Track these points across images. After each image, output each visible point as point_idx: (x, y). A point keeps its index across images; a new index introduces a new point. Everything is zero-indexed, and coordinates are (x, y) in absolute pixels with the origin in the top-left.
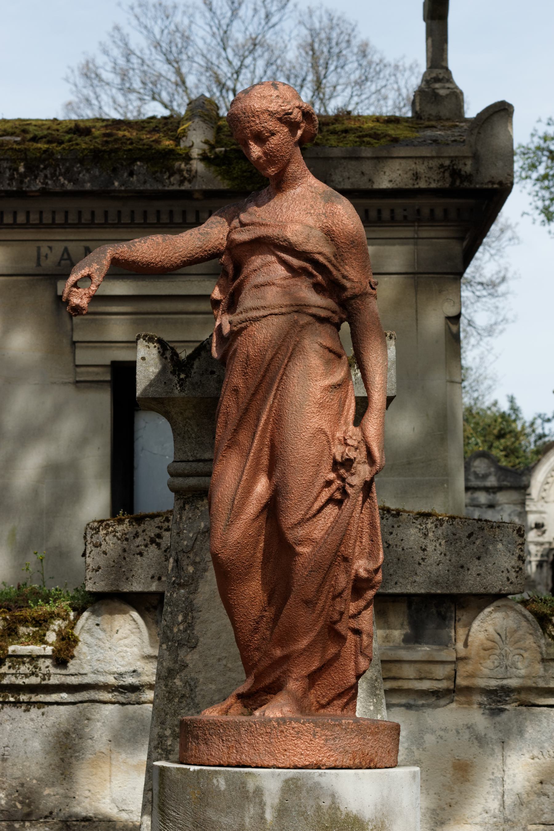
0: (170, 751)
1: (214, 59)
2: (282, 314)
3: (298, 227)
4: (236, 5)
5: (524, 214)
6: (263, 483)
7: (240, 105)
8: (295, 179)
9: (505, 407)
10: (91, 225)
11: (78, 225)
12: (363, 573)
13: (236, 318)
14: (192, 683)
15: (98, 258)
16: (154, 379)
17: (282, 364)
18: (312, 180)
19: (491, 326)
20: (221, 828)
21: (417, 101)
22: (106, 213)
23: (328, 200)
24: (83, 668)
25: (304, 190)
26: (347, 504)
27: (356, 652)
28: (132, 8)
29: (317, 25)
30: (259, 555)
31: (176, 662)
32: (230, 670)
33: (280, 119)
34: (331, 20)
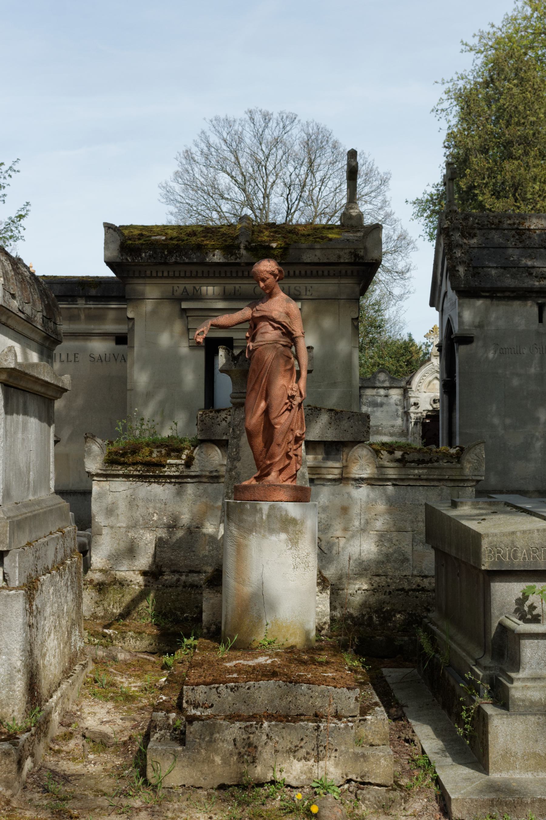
3: (277, 312)
5: (420, 236)
8: (276, 294)
9: (407, 338)
10: (196, 277)
11: (191, 277)
12: (298, 435)
13: (255, 344)
18: (282, 294)
19: (95, 586)
22: (203, 272)
23: (288, 301)
26: (293, 411)
28: (211, 121)
29: (311, 132)
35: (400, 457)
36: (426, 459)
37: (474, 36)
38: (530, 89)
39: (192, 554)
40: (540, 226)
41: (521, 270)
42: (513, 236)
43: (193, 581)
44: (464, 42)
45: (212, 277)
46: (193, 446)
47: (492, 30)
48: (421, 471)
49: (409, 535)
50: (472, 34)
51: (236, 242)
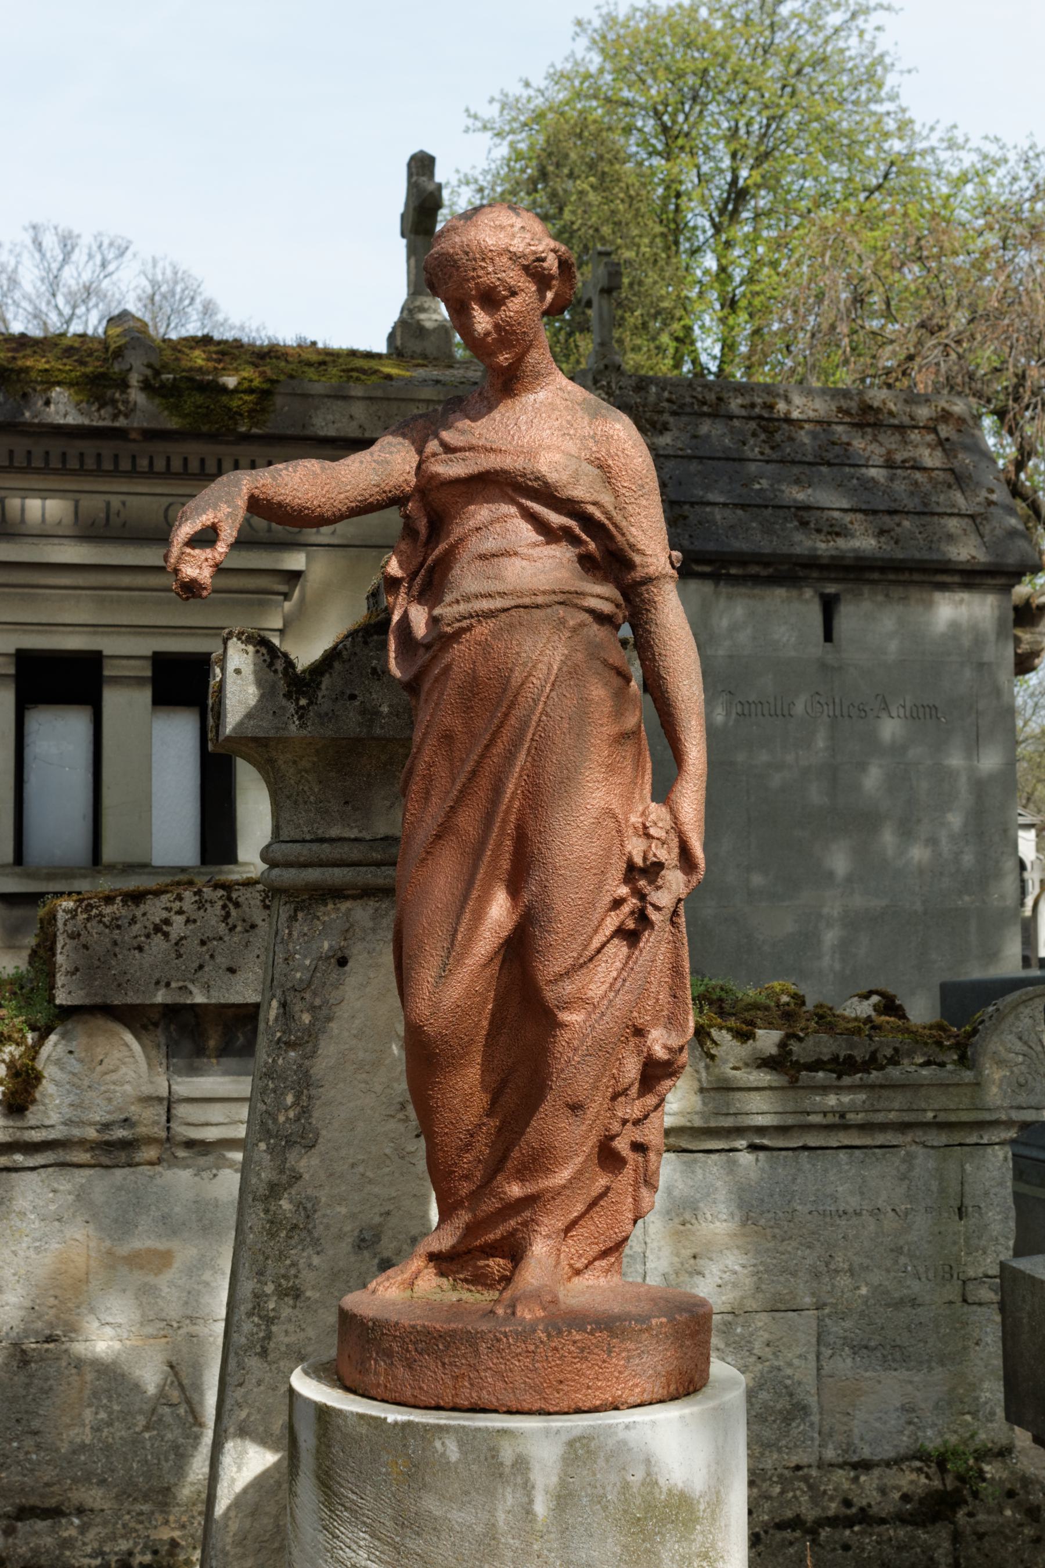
0: (274, 1318)
1: (44, 307)
3: (557, 457)
4: (69, 247)
6: (501, 901)
7: (457, 239)
8: (538, 376)
12: (660, 1053)
14: (309, 1206)
15: (228, 493)
16: (255, 706)
17: (540, 695)
20: (451, 1530)
21: (398, 333)
23: (595, 415)
24: (49, 1118)
25: (550, 395)
27: (636, 1181)
29: (160, 277)
30: (485, 1023)
31: (282, 1172)
32: (370, 1182)
33: (526, 268)
34: (176, 273)
35: (774, 1051)
36: (860, 1054)
37: (492, 100)
38: (622, 195)
39: (29, 1442)
40: (811, 414)
41: (781, 513)
42: (754, 435)
43: (36, 1552)
44: (472, 112)
45: (38, 471)
46: (33, 1028)
47: (526, 93)
48: (846, 1099)
49: (806, 1323)
50: (488, 98)
51: (116, 368)
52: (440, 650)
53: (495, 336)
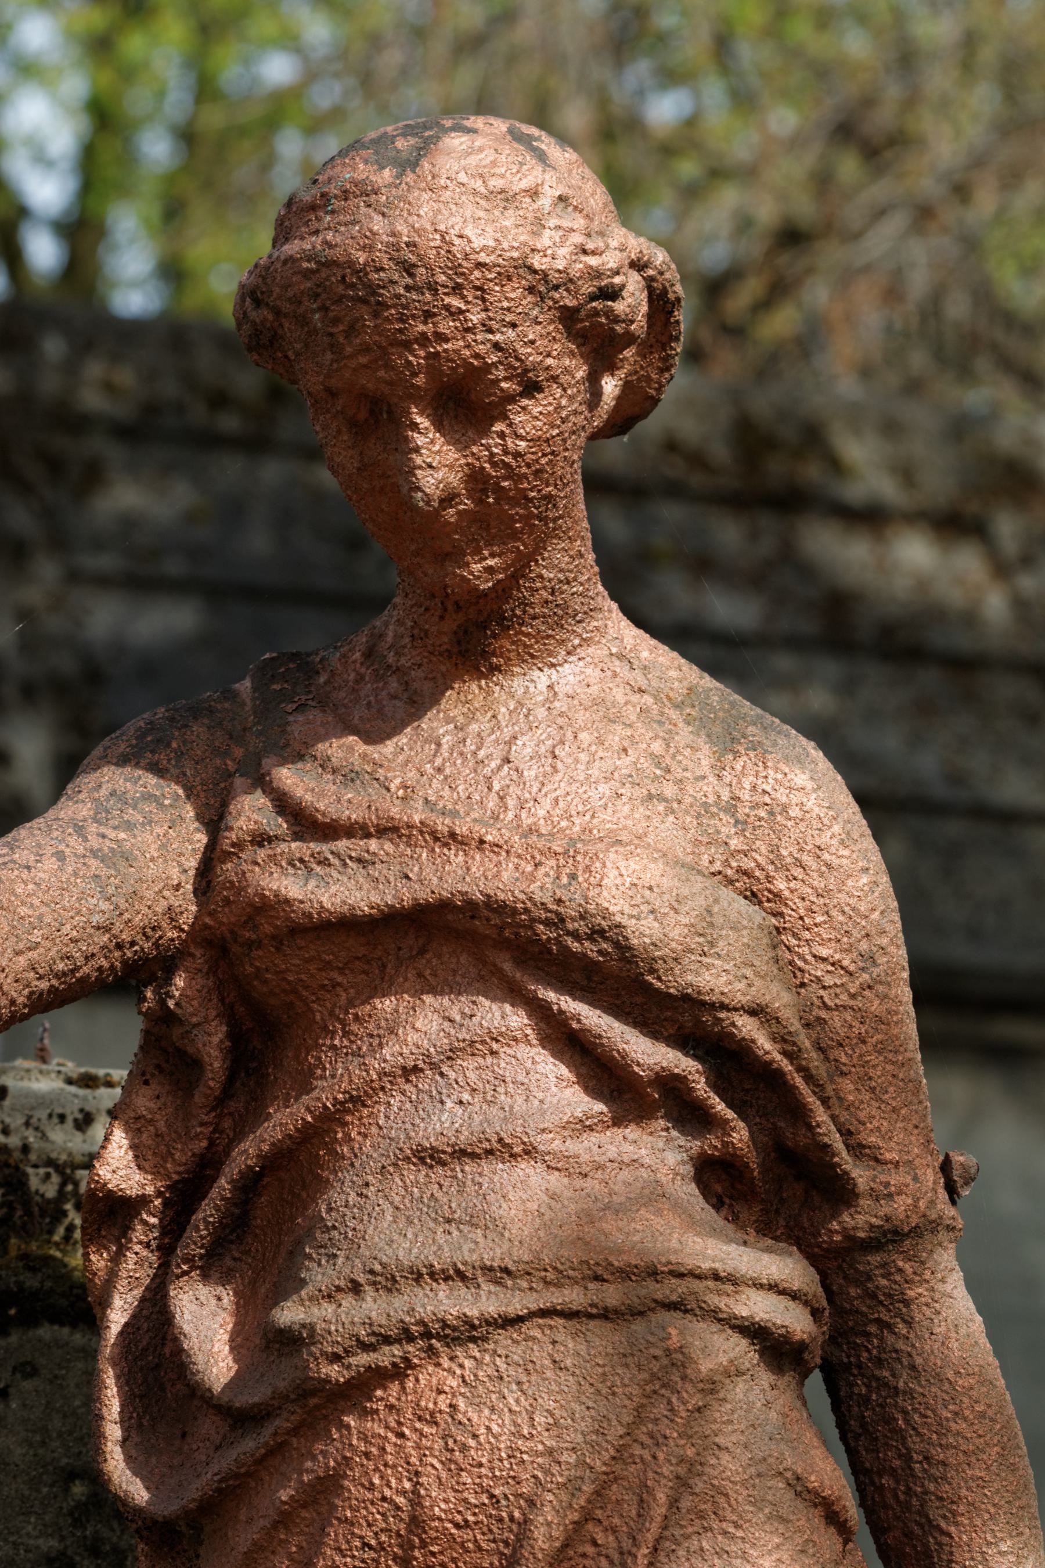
2: (606, 1315)
3: (654, 872)
7: (378, 224)
33: (568, 317)
52: (295, 1431)
53: (467, 504)
